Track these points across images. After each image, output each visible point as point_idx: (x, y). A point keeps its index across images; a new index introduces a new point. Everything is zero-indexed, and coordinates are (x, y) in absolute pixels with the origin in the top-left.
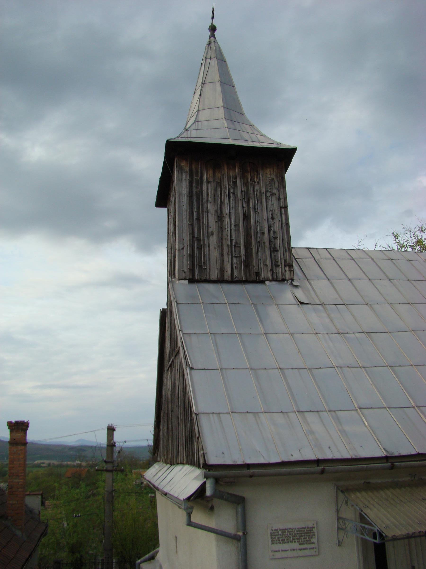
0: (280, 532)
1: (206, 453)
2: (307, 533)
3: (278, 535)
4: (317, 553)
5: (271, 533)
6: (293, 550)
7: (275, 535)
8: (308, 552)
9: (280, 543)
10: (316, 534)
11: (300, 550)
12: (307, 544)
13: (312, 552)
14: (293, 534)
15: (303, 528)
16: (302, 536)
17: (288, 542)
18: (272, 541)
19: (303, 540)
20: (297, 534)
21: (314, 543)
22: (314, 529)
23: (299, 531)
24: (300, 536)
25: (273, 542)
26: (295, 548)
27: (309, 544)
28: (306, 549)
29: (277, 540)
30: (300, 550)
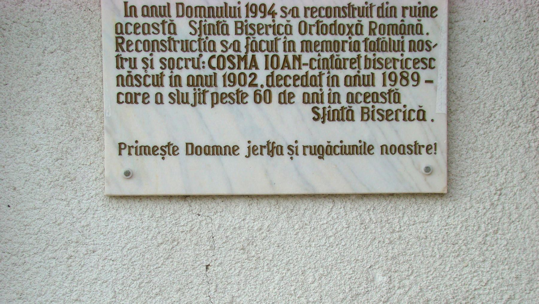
0: (183, 29)
1: (164, 75)
2: (373, 47)
3: (170, 44)
4: (438, 184)
5: (120, 30)
6: (273, 149)
7: (150, 46)
8: (371, 173)
9: (179, 99)
10: (440, 54)
11: (320, 151)
12: (367, 115)
13: (407, 173)
14: (272, 46)
15: (349, 10)
16: (340, 65)
17: (240, 98)
18: (121, 81)
19: (343, 91)
20: (307, 46)
21: (421, 115)
22: (426, 22)
23: (321, 29)
24: (325, 64)
25: (132, 89)
26: (284, 139)
27: (386, 116)
28: (365, 149)
29: (158, 81)
30: (320, 151)
